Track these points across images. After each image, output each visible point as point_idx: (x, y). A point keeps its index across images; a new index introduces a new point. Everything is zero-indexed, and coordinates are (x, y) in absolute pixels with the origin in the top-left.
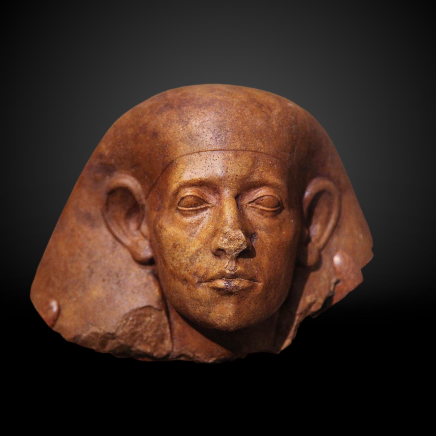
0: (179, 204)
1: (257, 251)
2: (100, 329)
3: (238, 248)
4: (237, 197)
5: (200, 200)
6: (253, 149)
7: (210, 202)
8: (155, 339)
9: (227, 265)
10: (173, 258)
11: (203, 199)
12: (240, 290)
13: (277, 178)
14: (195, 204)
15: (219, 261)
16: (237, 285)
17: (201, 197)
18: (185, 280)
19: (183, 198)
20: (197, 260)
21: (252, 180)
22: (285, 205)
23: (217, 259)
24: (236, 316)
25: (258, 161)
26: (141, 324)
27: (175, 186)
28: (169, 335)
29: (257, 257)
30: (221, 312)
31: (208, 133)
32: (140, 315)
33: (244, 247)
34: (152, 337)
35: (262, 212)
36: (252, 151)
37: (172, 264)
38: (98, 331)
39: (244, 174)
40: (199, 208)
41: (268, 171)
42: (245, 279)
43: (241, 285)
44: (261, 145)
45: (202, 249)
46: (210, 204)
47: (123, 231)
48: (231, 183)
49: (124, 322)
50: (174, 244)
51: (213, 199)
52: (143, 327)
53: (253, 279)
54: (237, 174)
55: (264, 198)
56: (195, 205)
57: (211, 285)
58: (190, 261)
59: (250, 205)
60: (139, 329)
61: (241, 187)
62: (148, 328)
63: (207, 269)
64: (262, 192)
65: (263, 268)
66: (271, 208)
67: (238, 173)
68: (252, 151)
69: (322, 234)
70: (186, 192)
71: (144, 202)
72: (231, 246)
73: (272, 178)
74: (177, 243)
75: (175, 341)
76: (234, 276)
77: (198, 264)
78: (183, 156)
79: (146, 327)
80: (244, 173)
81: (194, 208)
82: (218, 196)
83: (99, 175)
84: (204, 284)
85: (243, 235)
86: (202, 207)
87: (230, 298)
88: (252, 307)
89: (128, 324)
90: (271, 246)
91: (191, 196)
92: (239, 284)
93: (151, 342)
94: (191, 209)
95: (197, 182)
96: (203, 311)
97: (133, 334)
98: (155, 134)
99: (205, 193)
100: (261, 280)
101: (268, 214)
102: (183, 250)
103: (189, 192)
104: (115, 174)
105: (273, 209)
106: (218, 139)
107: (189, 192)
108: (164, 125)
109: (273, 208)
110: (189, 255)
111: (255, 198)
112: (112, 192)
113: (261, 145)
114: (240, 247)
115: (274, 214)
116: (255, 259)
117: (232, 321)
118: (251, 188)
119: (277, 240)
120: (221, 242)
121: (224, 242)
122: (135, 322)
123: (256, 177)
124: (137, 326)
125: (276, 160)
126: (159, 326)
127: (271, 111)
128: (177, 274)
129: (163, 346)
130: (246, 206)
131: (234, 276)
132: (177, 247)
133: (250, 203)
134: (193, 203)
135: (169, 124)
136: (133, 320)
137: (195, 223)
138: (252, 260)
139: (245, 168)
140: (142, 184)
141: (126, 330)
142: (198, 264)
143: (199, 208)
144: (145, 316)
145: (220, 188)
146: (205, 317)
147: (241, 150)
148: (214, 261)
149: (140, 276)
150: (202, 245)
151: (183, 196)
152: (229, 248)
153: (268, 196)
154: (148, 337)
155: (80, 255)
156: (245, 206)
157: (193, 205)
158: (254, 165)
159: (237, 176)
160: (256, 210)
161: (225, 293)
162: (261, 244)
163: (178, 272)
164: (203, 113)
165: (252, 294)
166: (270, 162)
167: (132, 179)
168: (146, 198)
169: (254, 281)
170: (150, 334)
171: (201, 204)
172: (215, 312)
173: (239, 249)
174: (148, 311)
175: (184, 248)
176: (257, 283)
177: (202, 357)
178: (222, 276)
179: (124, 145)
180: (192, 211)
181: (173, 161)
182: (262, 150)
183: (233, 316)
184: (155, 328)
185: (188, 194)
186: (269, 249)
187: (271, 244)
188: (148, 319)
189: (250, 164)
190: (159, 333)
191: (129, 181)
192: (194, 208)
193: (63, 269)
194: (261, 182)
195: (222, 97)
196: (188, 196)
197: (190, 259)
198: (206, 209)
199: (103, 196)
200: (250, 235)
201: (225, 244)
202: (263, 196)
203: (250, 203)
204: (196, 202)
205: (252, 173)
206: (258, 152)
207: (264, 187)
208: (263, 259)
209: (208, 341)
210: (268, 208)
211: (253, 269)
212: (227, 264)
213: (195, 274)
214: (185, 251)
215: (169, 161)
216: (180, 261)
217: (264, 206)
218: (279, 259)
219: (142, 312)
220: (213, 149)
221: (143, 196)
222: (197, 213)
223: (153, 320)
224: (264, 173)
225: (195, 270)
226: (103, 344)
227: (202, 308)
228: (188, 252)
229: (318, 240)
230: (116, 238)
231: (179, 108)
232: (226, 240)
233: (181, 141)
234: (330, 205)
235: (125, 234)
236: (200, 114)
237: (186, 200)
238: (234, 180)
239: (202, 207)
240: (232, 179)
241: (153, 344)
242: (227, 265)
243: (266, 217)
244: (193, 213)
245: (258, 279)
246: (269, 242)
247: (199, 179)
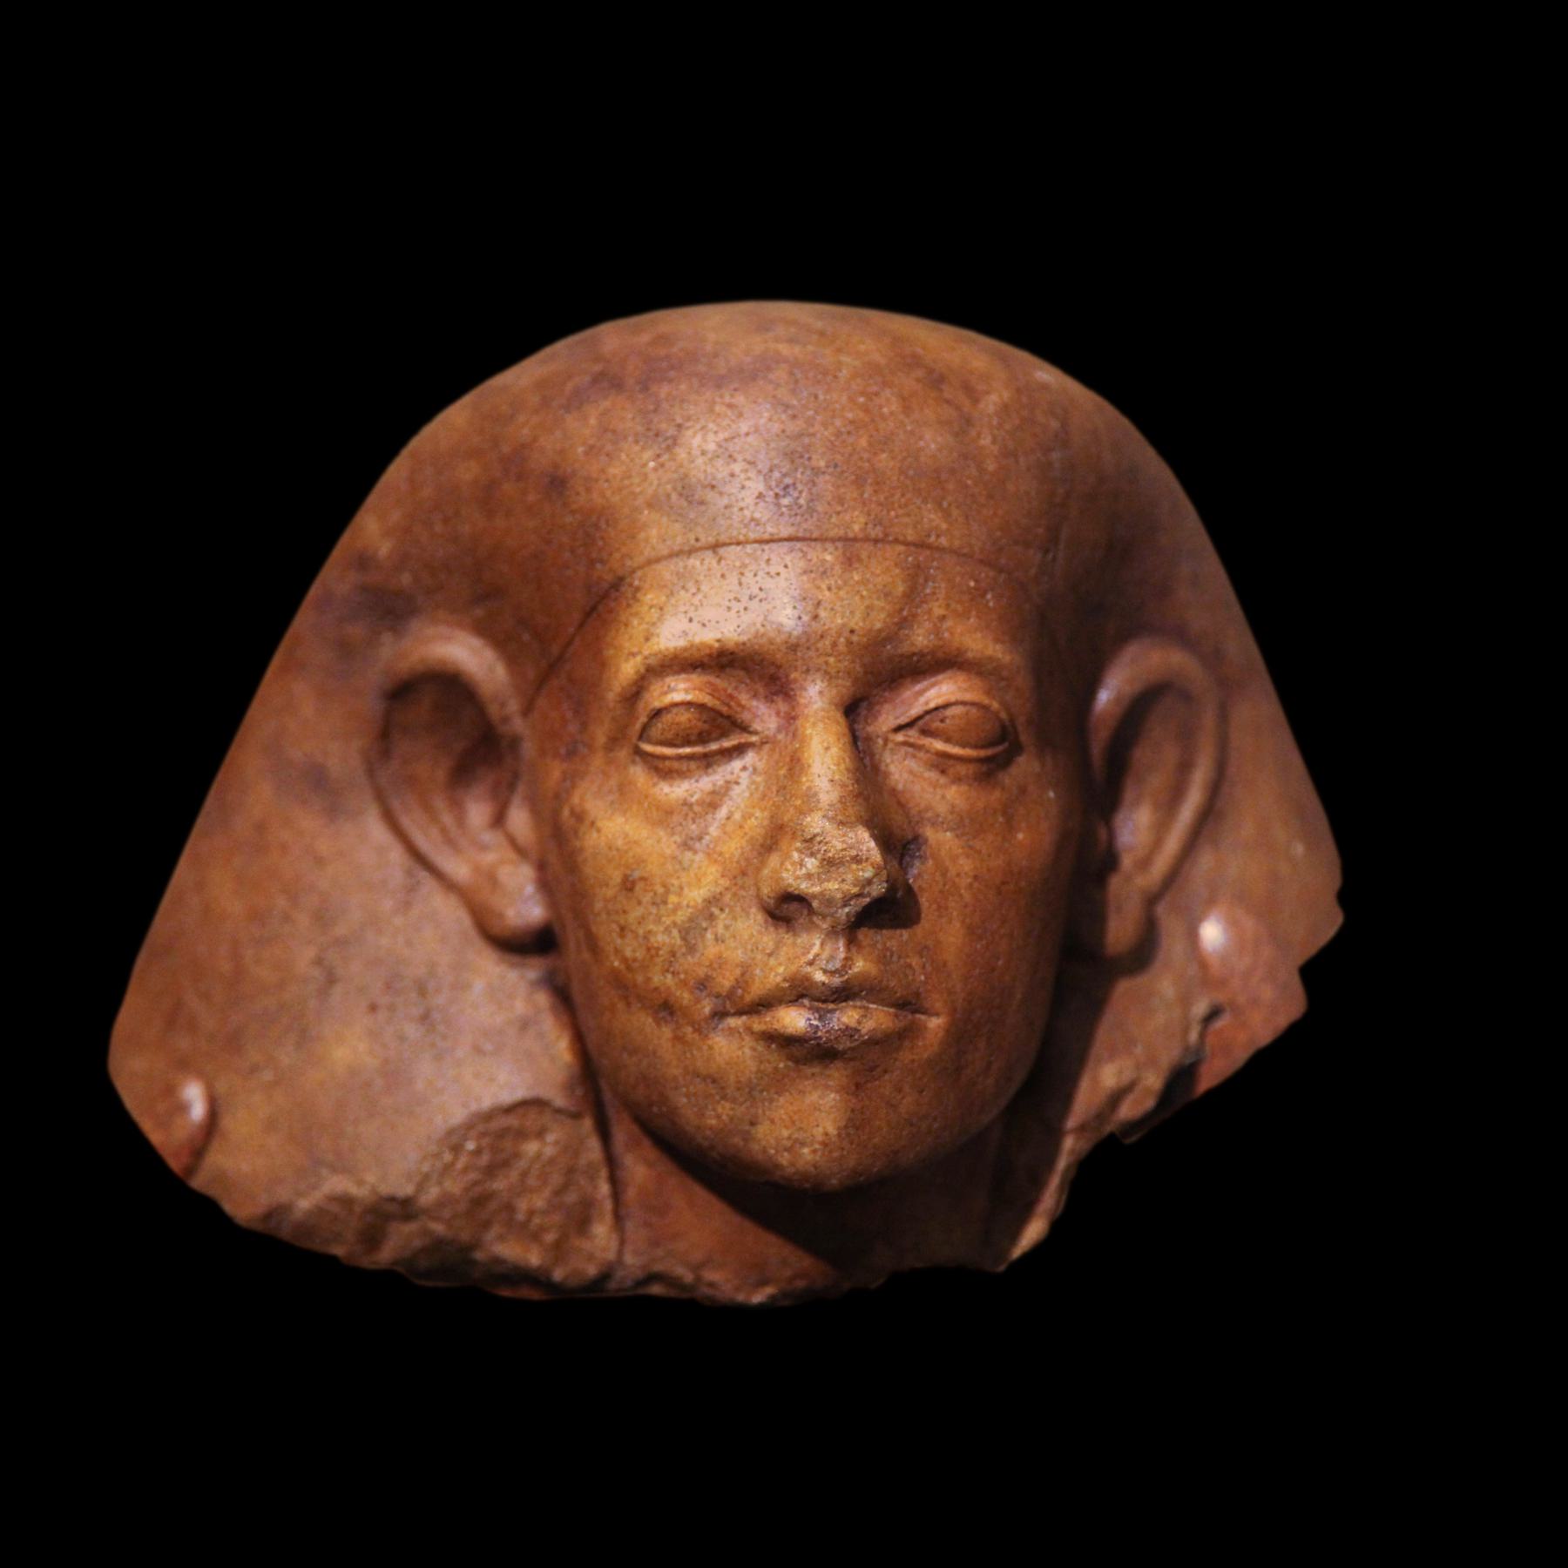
0: (643, 734)
1: (924, 901)
2: (360, 1183)
3: (855, 890)
4: (854, 710)
5: (720, 720)
6: (911, 535)
7: (756, 726)
8: (557, 1218)
9: (816, 954)
10: (622, 929)
11: (728, 717)
12: (864, 1043)
13: (997, 640)
14: (700, 734)
15: (788, 938)
16: (853, 1024)
17: (724, 709)
18: (666, 1009)
19: (657, 713)
20: (709, 935)
21: (905, 648)
22: (1023, 738)
23: (782, 931)
24: (848, 1135)
25: (926, 581)
26: (506, 1164)
27: (628, 669)
28: (608, 1205)
29: (925, 924)
30: (793, 1122)
31: (756, 484)
32: (502, 1134)
33: (878, 889)
34: (545, 1213)
35: (942, 763)
36: (907, 544)
37: (617, 951)
38: (354, 1190)
39: (878, 625)
40: (714, 746)
41: (965, 615)
42: (882, 1002)
43: (868, 1026)
44: (937, 521)
45: (727, 897)
46: (756, 733)
47: (444, 831)
48: (832, 660)
49: (448, 1157)
50: (626, 878)
51: (764, 717)
52: (514, 1175)
53: (908, 1004)
54: (852, 625)
55: (949, 712)
56: (702, 739)
57: (758, 1024)
58: (684, 939)
59: (900, 737)
60: (499, 1184)
61: (866, 673)
62: (532, 1181)
63: (746, 969)
64: (941, 691)
65: (945, 965)
66: (976, 747)
67: (856, 622)
68: (907, 544)
69: (1158, 843)
70: (670, 690)
71: (519, 725)
72: (833, 886)
73: (977, 641)
74: (637, 874)
75: (630, 1225)
76: (843, 994)
77: (710, 950)
78: (658, 560)
79: (524, 1174)
80: (879, 621)
81: (698, 749)
82: (783, 706)
83: (356, 631)
84: (733, 1022)
85: (872, 844)
86: (727, 743)
87: (828, 1072)
88: (907, 1103)
89: (460, 1165)
90: (976, 885)
91: (688, 704)
92: (859, 1022)
93: (542, 1229)
94: (688, 750)
95: (710, 655)
96: (731, 1119)
97: (480, 1201)
98: (557, 483)
99: (736, 694)
100: (938, 1005)
101: (962, 769)
102: (658, 900)
103: (679, 690)
104: (415, 625)
105: (983, 753)
106: (785, 501)
107: (679, 690)
108: (591, 451)
109: (983, 747)
110: (681, 917)
111: (915, 711)
112: (402, 691)
113: (937, 521)
114: (863, 887)
115: (984, 768)
116: (919, 930)
117: (835, 1154)
118: (901, 676)
119: (998, 862)
120: (796, 871)
121: (804, 871)
122: (485, 1159)
123: (920, 638)
124: (491, 1171)
125: (992, 574)
126: (570, 1171)
127: (976, 401)
128: (635, 986)
129: (586, 1245)
130: (886, 741)
131: (843, 994)
132: (637, 888)
133: (898, 729)
134: (696, 732)
135: (609, 447)
136: (478, 1152)
137: (700, 803)
138: (905, 934)
139: (880, 603)
140: (512, 661)
141: (454, 1186)
142: (710, 950)
143: (714, 746)
144: (521, 1135)
145: (793, 676)
146: (737, 1140)
147: (867, 539)
148: (768, 939)
150: (725, 882)
151: (657, 704)
152: (822, 893)
153: (964, 703)
154: (531, 1213)
155: (287, 918)
156: (880, 741)
157: (693, 738)
158: (913, 595)
159: (852, 631)
160: (921, 754)
161: (809, 1053)
162: (938, 877)
163: (640, 979)
164: (730, 406)
165: (905, 1056)
166: (972, 584)
167: (476, 642)
168: (527, 711)
169: (914, 1012)
170: (539, 1202)
171: (724, 734)
172: (772, 1121)
173: (858, 896)
174: (532, 1119)
175: (660, 890)
176: (923, 1017)
177: (726, 1283)
178: (799, 992)
179: (446, 520)
180: (690, 757)
181: (621, 579)
182: (943, 541)
183: (839, 1135)
184: (556, 1179)
185: (678, 697)
186: (967, 896)
187: (975, 877)
188: (531, 1147)
189: (901, 588)
190: (571, 1197)
191: (463, 651)
192: (698, 749)
193: (226, 967)
194: (940, 655)
195: (797, 349)
196: (676, 705)
197: (685, 933)
198: (740, 750)
199: (371, 705)
200: (898, 844)
201: (809, 876)
202: (946, 706)
203: (898, 729)
204: (706, 727)
205: (905, 621)
206: (929, 547)
207: (949, 673)
208: (945, 933)
209: (748, 1225)
210: (963, 746)
211: (910, 966)
212: (816, 949)
213: (703, 985)
214: (665, 903)
215: (609, 577)
216: (646, 938)
217: (948, 740)
218: (1002, 931)
219: (512, 1121)
220: (766, 536)
221: (513, 706)
222: (708, 766)
223: (549, 1151)
224: (949, 623)
225: (702, 972)
226: (372, 1237)
227: (725, 1109)
228: (677, 907)
229: (1145, 863)
230: (419, 858)
231: (645, 389)
232: (811, 864)
233: (650, 505)
234: (1186, 737)
235: (450, 842)
236: (718, 408)
237: (667, 718)
238: (842, 647)
239: (727, 743)
240: (834, 644)
241: (550, 1237)
242: (816, 954)
243: (958, 780)
244: (693, 765)
245: (927, 1005)
246: (966, 869)
247: (717, 645)
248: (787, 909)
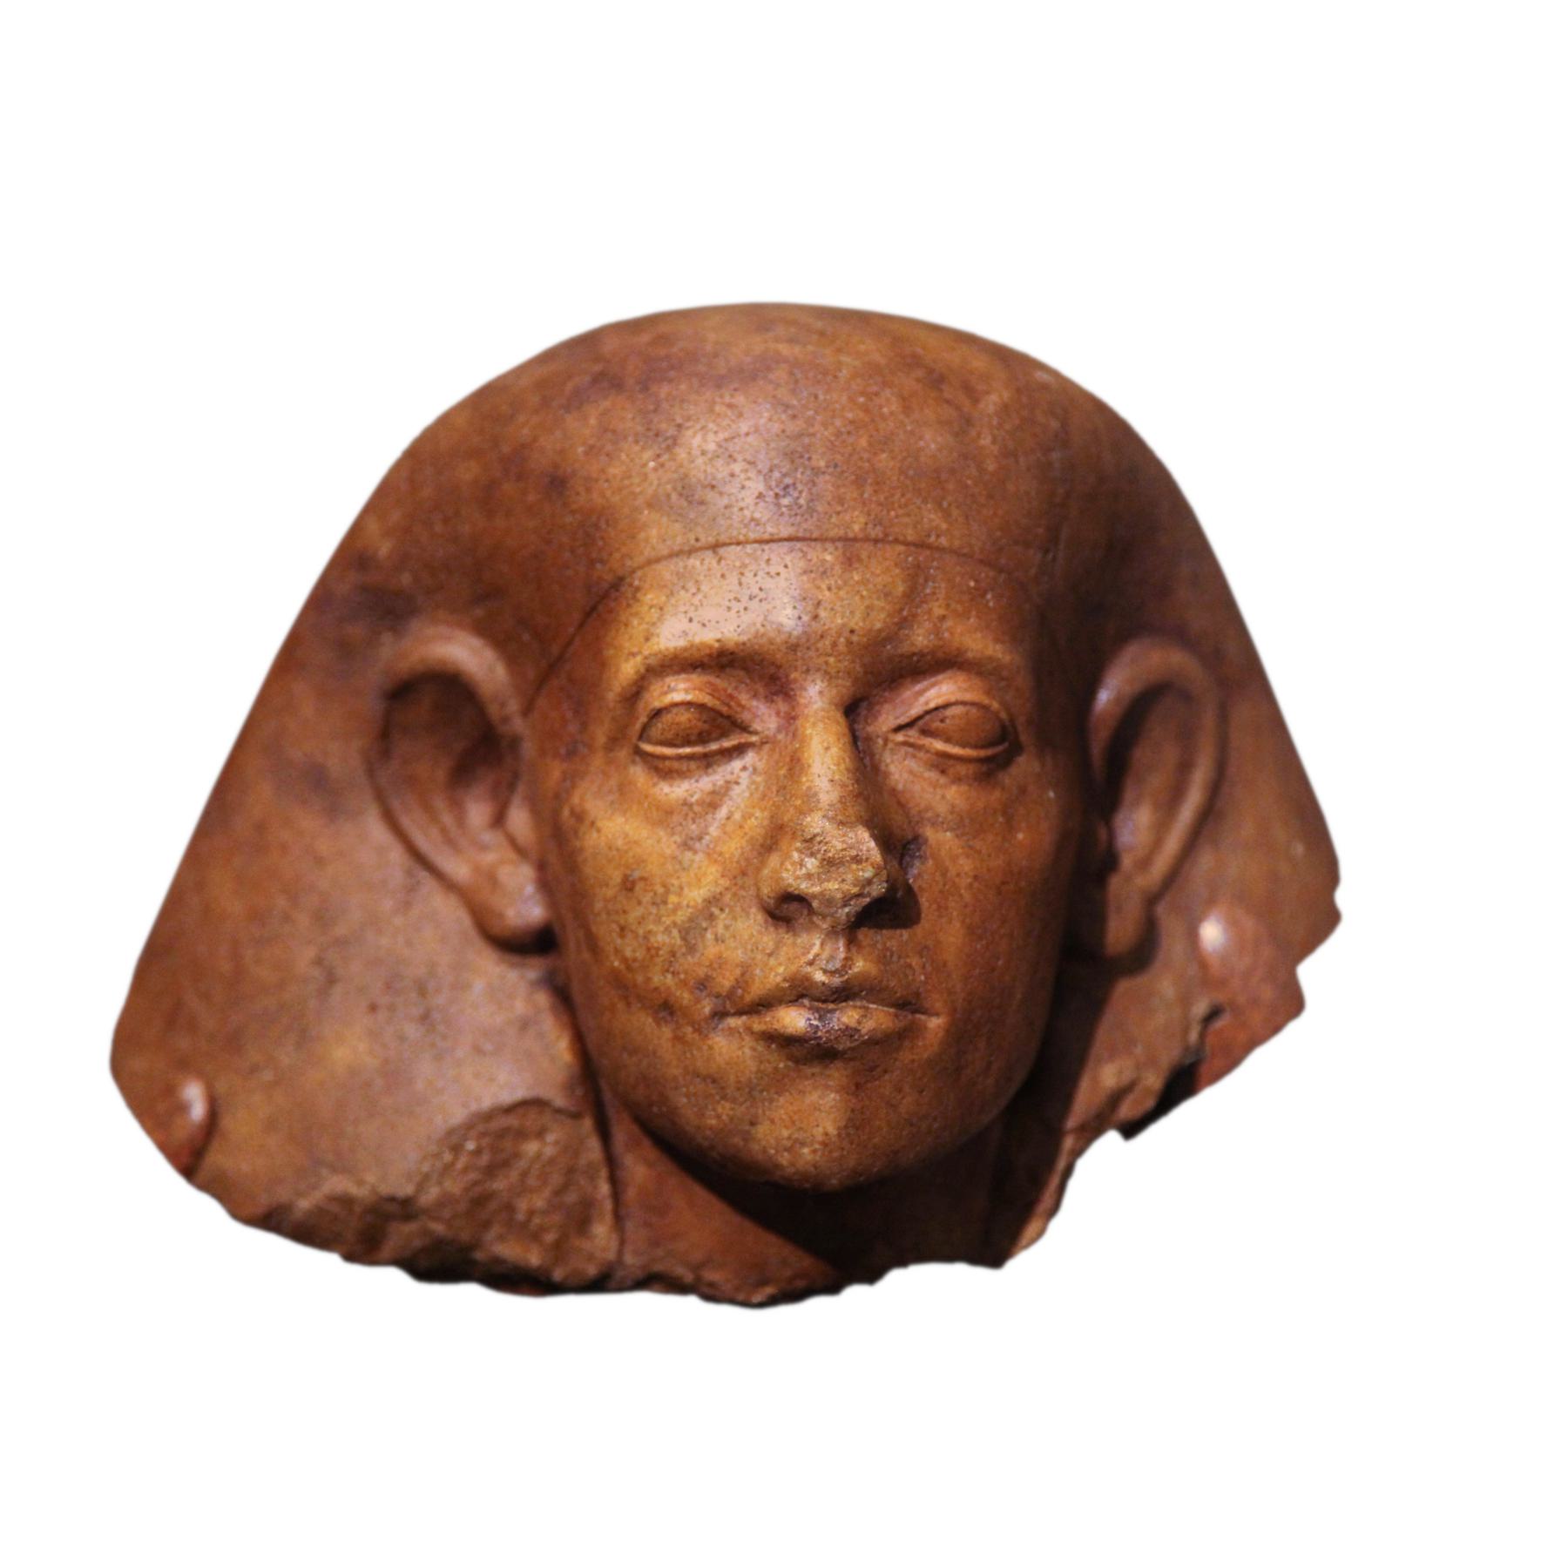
0: (643, 734)
1: (924, 901)
2: (360, 1183)
3: (855, 890)
4: (854, 710)
5: (720, 720)
6: (911, 535)
7: (756, 726)
8: (557, 1218)
9: (816, 954)
10: (622, 929)
11: (728, 717)
12: (864, 1043)
13: (997, 640)
14: (700, 734)
15: (788, 938)
16: (853, 1024)
17: (724, 709)
18: (666, 1009)
19: (657, 713)
20: (709, 935)
21: (905, 648)
22: (1023, 738)
23: (782, 931)
24: (848, 1135)
25: (926, 581)
26: (506, 1164)
27: (628, 669)
28: (608, 1205)
29: (925, 924)
30: (793, 1122)
32: (502, 1134)
33: (878, 889)
34: (545, 1213)
35: (942, 763)
36: (907, 544)
37: (617, 951)
38: (354, 1190)
39: (878, 625)
40: (714, 746)
41: (965, 615)
42: (882, 1002)
43: (868, 1026)
44: (937, 521)
45: (727, 897)
46: (756, 733)
47: (444, 831)
48: (832, 660)
49: (448, 1157)
50: (626, 878)
51: (764, 717)
52: (514, 1175)
53: (908, 1004)
54: (852, 625)
55: (949, 712)
56: (702, 739)
57: (758, 1024)
58: (684, 939)
59: (900, 737)
60: (499, 1184)
61: (866, 673)
62: (532, 1181)
63: (746, 969)
64: (941, 691)
65: (945, 965)
66: (976, 747)
67: (856, 622)
68: (907, 544)
69: (1158, 843)
70: (670, 690)
71: (519, 725)
72: (833, 886)
73: (977, 641)
74: (637, 874)
75: (630, 1225)
76: (843, 994)
77: (710, 950)
78: (658, 560)
79: (524, 1174)
80: (879, 621)
81: (698, 749)
82: (783, 706)
83: (356, 631)
84: (733, 1022)
85: (872, 844)
86: (727, 743)
87: (828, 1072)
88: (907, 1103)
89: (460, 1165)
90: (976, 885)
91: (688, 704)
92: (859, 1022)
93: (542, 1229)
94: (688, 750)
95: (710, 655)
96: (731, 1119)
97: (480, 1201)
98: (557, 483)
99: (736, 694)
100: (938, 1005)
101: (962, 769)
102: (658, 900)
103: (679, 690)
104: (415, 625)
105: (983, 753)
106: (785, 501)
107: (679, 690)
108: (591, 451)
109: (983, 747)
110: (681, 917)
111: (915, 711)
112: (402, 691)
113: (937, 521)
114: (863, 887)
115: (984, 768)
116: (919, 930)
117: (835, 1154)
118: (901, 676)
119: (998, 862)
120: (796, 871)
121: (804, 871)
122: (485, 1159)
123: (920, 638)
124: (491, 1171)
125: (992, 574)
126: (570, 1171)
127: (976, 401)
128: (635, 986)
129: (586, 1245)
130: (886, 741)
131: (843, 994)
132: (637, 888)
133: (898, 729)
134: (696, 732)
135: (609, 447)
136: (478, 1152)
137: (700, 803)
138: (905, 934)
139: (880, 603)
140: (512, 661)
141: (454, 1186)
142: (710, 950)
143: (714, 746)
144: (521, 1135)
145: (793, 676)
146: (737, 1140)
147: (867, 539)
148: (768, 939)
150: (725, 882)
151: (657, 704)
152: (822, 893)
153: (964, 703)
154: (531, 1213)
155: (287, 918)
156: (880, 741)
157: (693, 738)
158: (913, 595)
159: (852, 631)
160: (921, 754)
161: (809, 1053)
162: (938, 877)
163: (640, 979)
164: (730, 406)
165: (905, 1056)
166: (972, 584)
167: (476, 642)
168: (527, 711)
169: (914, 1012)
170: (539, 1202)
171: (724, 734)
172: (772, 1121)
173: (858, 896)
174: (532, 1119)
175: (660, 890)
176: (923, 1017)
178: (799, 992)
179: (446, 520)
180: (690, 757)
181: (621, 579)
182: (943, 541)
183: (839, 1135)
184: (556, 1179)
185: (678, 697)
186: (967, 896)
187: (975, 877)
188: (531, 1147)
189: (901, 588)
190: (571, 1197)
191: (463, 651)
192: (698, 749)
193: (226, 967)
194: (940, 655)
195: (797, 349)
196: (676, 705)
197: (685, 933)
198: (740, 750)
199: (371, 705)
200: (898, 844)
201: (809, 876)
202: (946, 706)
203: (898, 729)
204: (706, 727)
205: (905, 621)
206: (929, 547)
207: (949, 673)
209: (748, 1225)
211: (910, 966)
212: (816, 949)
213: (703, 985)
214: (665, 903)
215: (609, 577)
216: (646, 938)
217: (948, 740)
218: (1002, 931)
220: (766, 536)
221: (513, 706)
222: (708, 766)
223: (549, 1151)
224: (949, 623)
225: (702, 972)
227: (725, 1109)
228: (677, 907)
229: (1145, 863)
230: (419, 858)
231: (645, 389)
232: (811, 864)
233: (650, 505)
234: (1186, 737)
235: (450, 842)
236: (718, 408)
237: (667, 718)
238: (842, 647)
239: (727, 743)
240: (834, 644)
241: (550, 1237)
242: (816, 954)
243: (958, 780)
244: (693, 765)
245: (927, 1005)
246: (966, 869)
247: (717, 645)
248: (787, 909)
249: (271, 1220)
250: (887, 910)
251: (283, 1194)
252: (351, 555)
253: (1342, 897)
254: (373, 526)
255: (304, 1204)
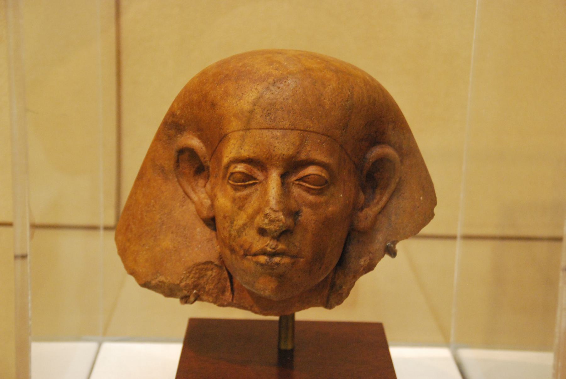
0: (229, 179)
2: (166, 279)
4: (283, 176)
6: (302, 128)
7: (258, 178)
8: (216, 291)
9: (269, 244)
10: (224, 228)
15: (262, 238)
16: (278, 262)
17: (250, 174)
19: (232, 174)
20: (244, 233)
21: (299, 159)
25: (306, 140)
26: (203, 277)
27: (226, 160)
28: (230, 288)
32: (202, 269)
34: (213, 289)
36: (300, 130)
38: (165, 281)
39: (291, 153)
40: (247, 183)
45: (248, 224)
46: (258, 180)
47: (192, 187)
49: (188, 275)
50: (224, 215)
51: (260, 176)
52: (205, 279)
54: (284, 153)
55: (311, 176)
56: (243, 181)
57: (255, 259)
59: (297, 182)
60: (202, 281)
62: (209, 281)
63: (252, 244)
64: (311, 170)
67: (285, 152)
68: (300, 130)
70: (235, 167)
72: (272, 227)
75: (235, 293)
77: (244, 238)
78: (235, 131)
79: (208, 280)
80: (291, 152)
81: (243, 184)
82: (265, 174)
84: (249, 257)
86: (251, 182)
89: (191, 276)
91: (240, 172)
93: (212, 293)
94: (240, 184)
98: (213, 105)
101: (314, 192)
103: (240, 168)
104: (185, 133)
106: (268, 118)
107: (240, 168)
108: (222, 98)
110: (237, 227)
112: (182, 151)
122: (197, 276)
123: (303, 156)
124: (199, 278)
126: (220, 279)
127: (325, 88)
129: (223, 297)
130: (293, 183)
135: (225, 98)
136: (196, 273)
137: (243, 198)
139: (292, 147)
140: (206, 146)
141: (189, 282)
142: (244, 238)
143: (247, 183)
144: (207, 270)
147: (289, 129)
148: (257, 237)
149: (202, 232)
150: (248, 220)
151: (234, 171)
152: (269, 229)
153: (314, 175)
154: (209, 289)
155: (153, 206)
164: (256, 89)
167: (199, 141)
168: (210, 161)
170: (212, 287)
174: (209, 266)
178: (264, 253)
179: (190, 109)
180: (241, 186)
181: (226, 135)
182: (311, 129)
184: (216, 281)
185: (237, 170)
188: (209, 273)
189: (298, 143)
190: (220, 286)
191: (195, 142)
192: (243, 184)
193: (139, 217)
195: (277, 72)
196: (237, 172)
197: (238, 232)
198: (254, 184)
199: (174, 153)
200: (294, 214)
201: (266, 224)
202: (310, 175)
203: (297, 180)
205: (298, 153)
206: (307, 131)
208: (303, 242)
210: (317, 186)
212: (268, 242)
213: (241, 246)
215: (223, 134)
217: (310, 184)
219: (205, 267)
221: (207, 159)
223: (214, 274)
224: (311, 152)
225: (242, 243)
228: (236, 224)
230: (186, 193)
231: (236, 82)
232: (266, 221)
233: (234, 116)
235: (193, 190)
236: (253, 90)
237: (235, 175)
239: (251, 182)
240: (279, 158)
241: (214, 295)
242: (269, 244)
243: (312, 194)
248: (262, 232)
249: (145, 285)
250: (284, 234)
251: (149, 279)
252: (171, 114)
253: (436, 210)
254: (176, 104)
255: (153, 282)
